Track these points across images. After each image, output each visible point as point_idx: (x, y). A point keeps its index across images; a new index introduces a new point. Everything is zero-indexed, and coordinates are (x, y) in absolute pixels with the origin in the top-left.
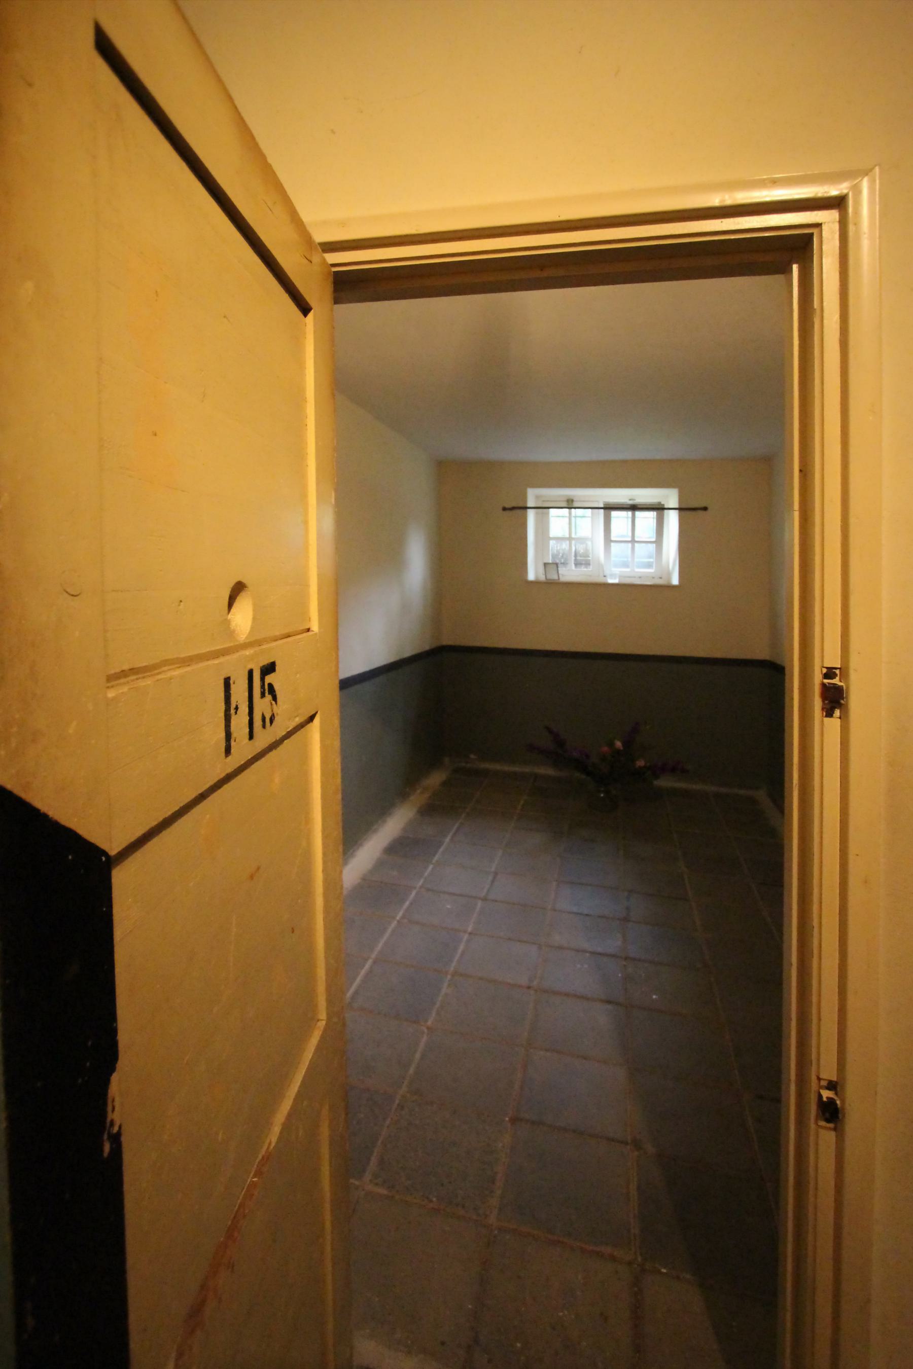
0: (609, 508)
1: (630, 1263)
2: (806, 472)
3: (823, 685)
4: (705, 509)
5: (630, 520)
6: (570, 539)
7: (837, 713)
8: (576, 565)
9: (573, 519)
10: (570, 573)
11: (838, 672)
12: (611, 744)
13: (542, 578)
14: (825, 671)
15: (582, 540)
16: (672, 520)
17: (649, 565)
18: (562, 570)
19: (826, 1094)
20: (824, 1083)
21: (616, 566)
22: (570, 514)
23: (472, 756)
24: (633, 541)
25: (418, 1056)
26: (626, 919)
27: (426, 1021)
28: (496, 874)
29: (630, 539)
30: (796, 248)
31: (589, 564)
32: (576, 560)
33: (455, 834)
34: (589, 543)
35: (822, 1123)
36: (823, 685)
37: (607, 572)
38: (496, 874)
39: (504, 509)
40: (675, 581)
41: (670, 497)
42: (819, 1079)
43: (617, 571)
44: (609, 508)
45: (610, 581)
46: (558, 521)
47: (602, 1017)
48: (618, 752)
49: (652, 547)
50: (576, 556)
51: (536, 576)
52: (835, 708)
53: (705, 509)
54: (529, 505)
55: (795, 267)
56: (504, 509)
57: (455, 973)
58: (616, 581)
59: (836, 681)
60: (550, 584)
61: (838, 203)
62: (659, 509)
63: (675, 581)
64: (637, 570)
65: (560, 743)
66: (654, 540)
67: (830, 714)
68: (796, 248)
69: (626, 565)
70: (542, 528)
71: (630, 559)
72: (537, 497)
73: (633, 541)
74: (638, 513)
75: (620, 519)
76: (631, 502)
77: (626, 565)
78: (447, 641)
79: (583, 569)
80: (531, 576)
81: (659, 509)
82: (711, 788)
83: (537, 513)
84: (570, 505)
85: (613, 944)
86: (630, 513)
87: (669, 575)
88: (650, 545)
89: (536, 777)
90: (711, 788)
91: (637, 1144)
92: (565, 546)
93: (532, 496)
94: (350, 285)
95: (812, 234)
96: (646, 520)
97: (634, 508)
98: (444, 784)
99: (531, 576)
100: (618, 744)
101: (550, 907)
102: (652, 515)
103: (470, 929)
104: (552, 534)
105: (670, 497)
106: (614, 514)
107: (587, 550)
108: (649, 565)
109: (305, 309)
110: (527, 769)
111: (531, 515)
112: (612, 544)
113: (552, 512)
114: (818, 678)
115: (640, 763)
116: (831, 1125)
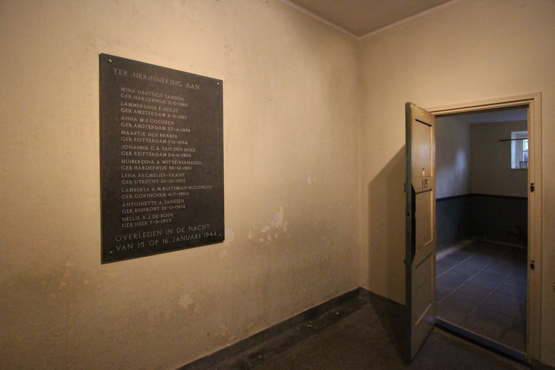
13: (519, 167)
68: (527, 106)
72: (517, 135)
80: (513, 166)
94: (437, 116)
99: (513, 166)
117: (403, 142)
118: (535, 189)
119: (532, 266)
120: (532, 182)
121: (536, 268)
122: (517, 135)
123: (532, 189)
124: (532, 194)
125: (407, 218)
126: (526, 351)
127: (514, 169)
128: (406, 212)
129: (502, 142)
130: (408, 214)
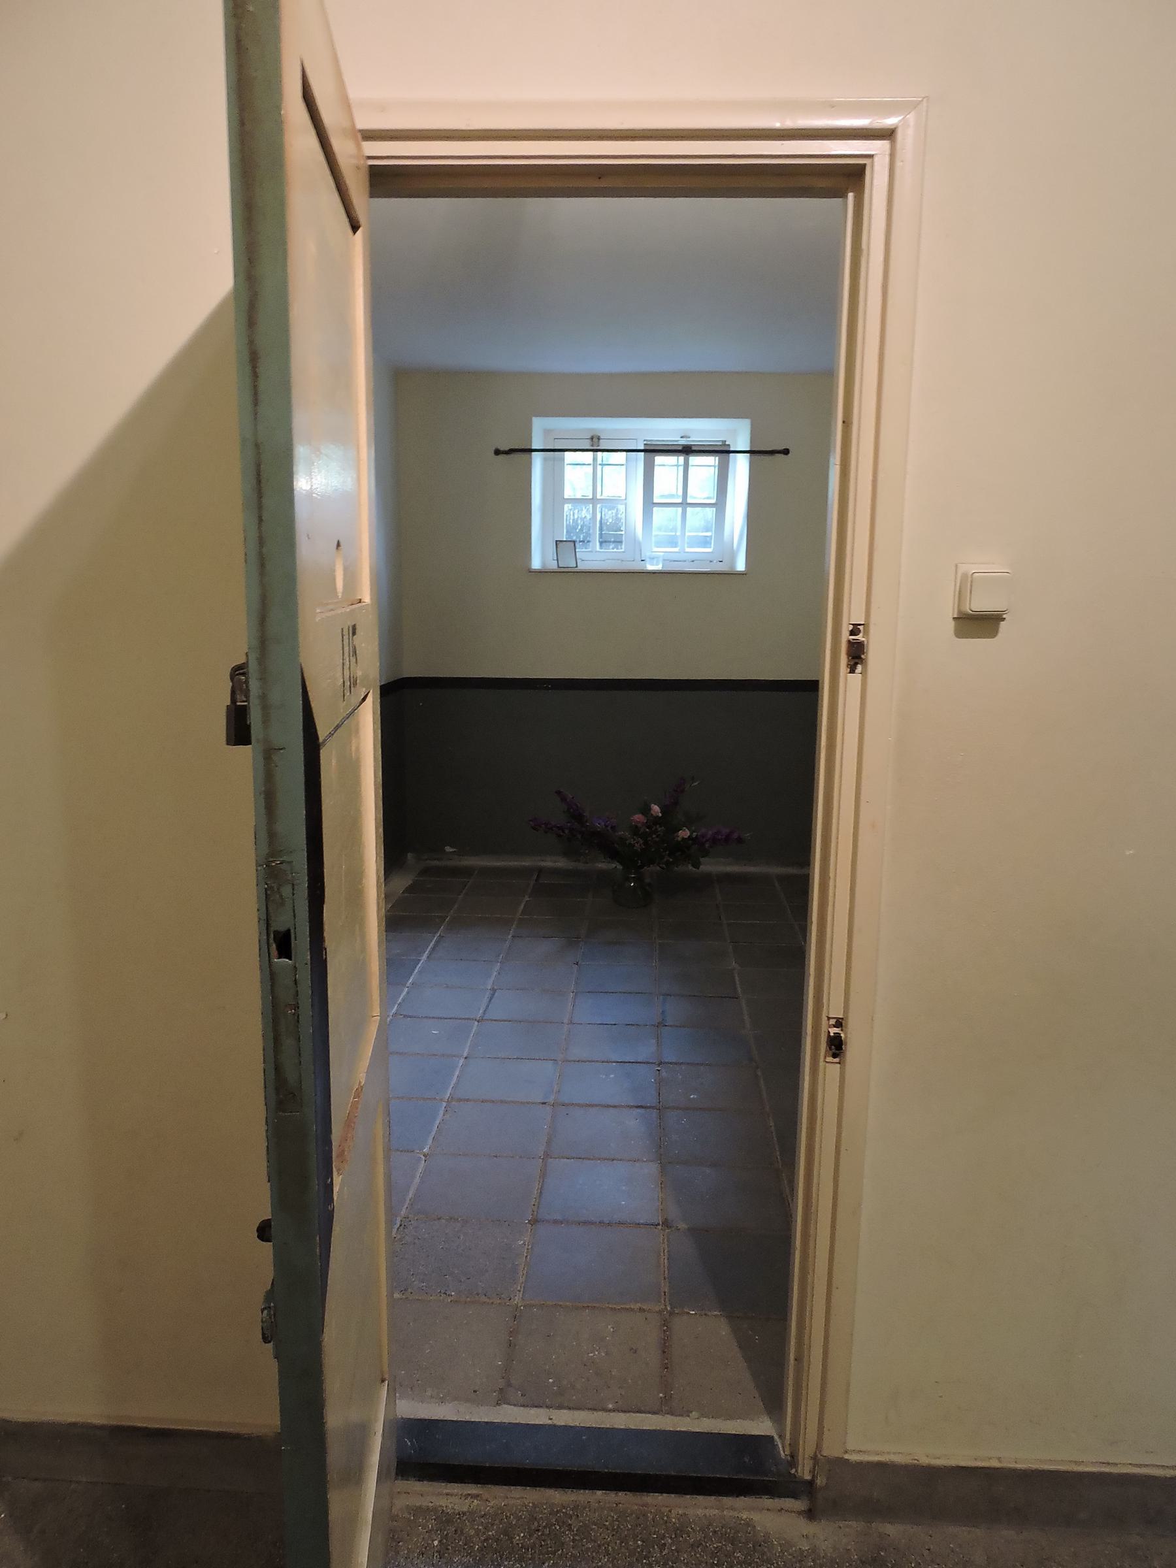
0: (652, 451)
1: (660, 1312)
2: (847, 423)
3: (849, 641)
4: (786, 452)
5: (681, 469)
6: (594, 500)
7: (859, 668)
8: (601, 543)
9: (599, 468)
10: (593, 557)
11: (861, 628)
12: (646, 810)
13: (553, 565)
14: (851, 627)
15: (611, 502)
16: (741, 466)
17: (705, 542)
18: (581, 551)
19: (833, 1031)
20: (833, 1022)
21: (658, 545)
22: (595, 459)
23: (448, 849)
24: (684, 504)
25: (417, 1180)
26: (661, 1024)
27: (421, 1149)
28: (494, 991)
29: (680, 501)
30: (848, 178)
31: (621, 542)
32: (601, 535)
33: (433, 949)
34: (621, 508)
35: (830, 1059)
36: (849, 641)
37: (646, 554)
38: (494, 991)
39: (497, 452)
40: (741, 566)
41: (739, 434)
42: (829, 1018)
43: (660, 551)
44: (652, 451)
45: (650, 567)
46: (577, 474)
47: (633, 1122)
48: (657, 821)
49: (710, 513)
50: (601, 529)
51: (543, 563)
52: (856, 664)
53: (786, 452)
54: (534, 447)
55: (851, 195)
56: (497, 452)
57: (451, 1098)
58: (659, 567)
59: (860, 637)
60: (563, 573)
61: (888, 134)
62: (723, 451)
63: (741, 566)
64: (687, 550)
65: (577, 816)
66: (713, 501)
67: (852, 671)
68: (848, 178)
69: (673, 542)
70: (555, 481)
71: (678, 533)
72: (547, 432)
73: (684, 504)
74: (694, 460)
75: (667, 468)
76: (683, 442)
77: (673, 542)
78: (408, 673)
79: (611, 549)
80: (536, 564)
81: (723, 451)
82: (776, 870)
83: (545, 459)
84: (595, 445)
85: (646, 1050)
86: (682, 459)
87: (733, 557)
88: (708, 509)
89: (540, 871)
90: (776, 870)
91: (666, 1224)
92: (585, 513)
93: (541, 431)
94: (387, 180)
95: (865, 165)
96: (704, 468)
97: (687, 450)
98: (409, 890)
99: (536, 564)
100: (656, 809)
101: (566, 1021)
102: (712, 460)
103: (465, 1055)
104: (568, 494)
105: (739, 434)
106: (659, 459)
107: (618, 519)
108: (705, 542)
109: (355, 228)
110: (527, 862)
111: (537, 460)
112: (655, 509)
113: (569, 457)
114: (845, 636)
115: (684, 833)
116: (837, 1060)
117: (218, 278)
118: (873, 655)
119: (837, 1046)
120: (854, 614)
121: (852, 1050)
122: (547, 432)
123: (857, 654)
124: (851, 683)
125: (271, 978)
126: (773, 1404)
127: (531, 571)
128: (267, 921)
129: (501, 457)
130: (283, 944)
